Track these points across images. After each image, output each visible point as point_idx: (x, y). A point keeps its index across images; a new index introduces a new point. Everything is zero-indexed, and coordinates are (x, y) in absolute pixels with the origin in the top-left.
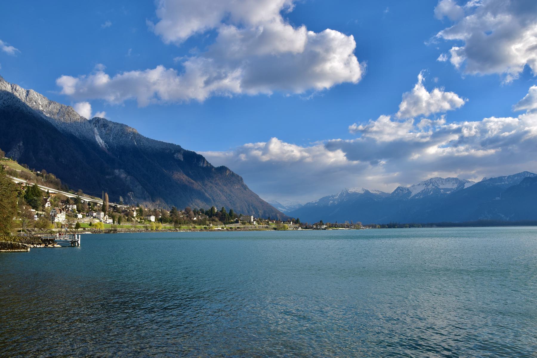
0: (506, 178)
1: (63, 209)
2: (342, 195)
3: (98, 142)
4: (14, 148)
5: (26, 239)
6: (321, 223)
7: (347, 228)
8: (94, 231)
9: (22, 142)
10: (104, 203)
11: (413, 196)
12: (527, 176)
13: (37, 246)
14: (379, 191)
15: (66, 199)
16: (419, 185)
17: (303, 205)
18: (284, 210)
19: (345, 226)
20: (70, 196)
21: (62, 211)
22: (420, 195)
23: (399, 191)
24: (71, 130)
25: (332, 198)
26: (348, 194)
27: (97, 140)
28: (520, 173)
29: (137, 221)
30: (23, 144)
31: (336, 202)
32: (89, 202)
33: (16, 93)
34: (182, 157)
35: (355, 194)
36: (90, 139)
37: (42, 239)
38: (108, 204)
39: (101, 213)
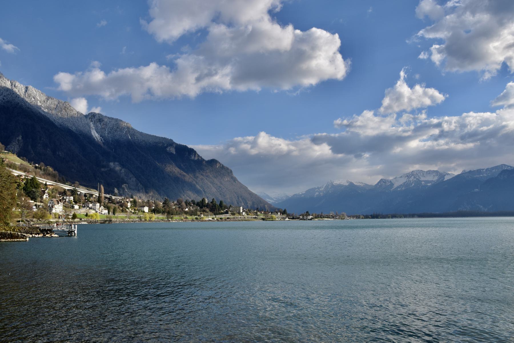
0: (484, 170)
1: (60, 201)
3: (94, 136)
5: (25, 230)
6: (308, 214)
7: (332, 218)
8: (90, 222)
9: (21, 136)
12: (504, 168)
13: (36, 236)
14: (362, 183)
16: (401, 177)
17: (290, 197)
19: (331, 216)
20: (67, 187)
21: (60, 202)
22: (402, 187)
24: (68, 125)
30: (22, 138)
31: (322, 194)
34: (174, 151)
35: (340, 186)
36: (86, 133)
37: (40, 229)
38: (103, 195)
39: (97, 204)
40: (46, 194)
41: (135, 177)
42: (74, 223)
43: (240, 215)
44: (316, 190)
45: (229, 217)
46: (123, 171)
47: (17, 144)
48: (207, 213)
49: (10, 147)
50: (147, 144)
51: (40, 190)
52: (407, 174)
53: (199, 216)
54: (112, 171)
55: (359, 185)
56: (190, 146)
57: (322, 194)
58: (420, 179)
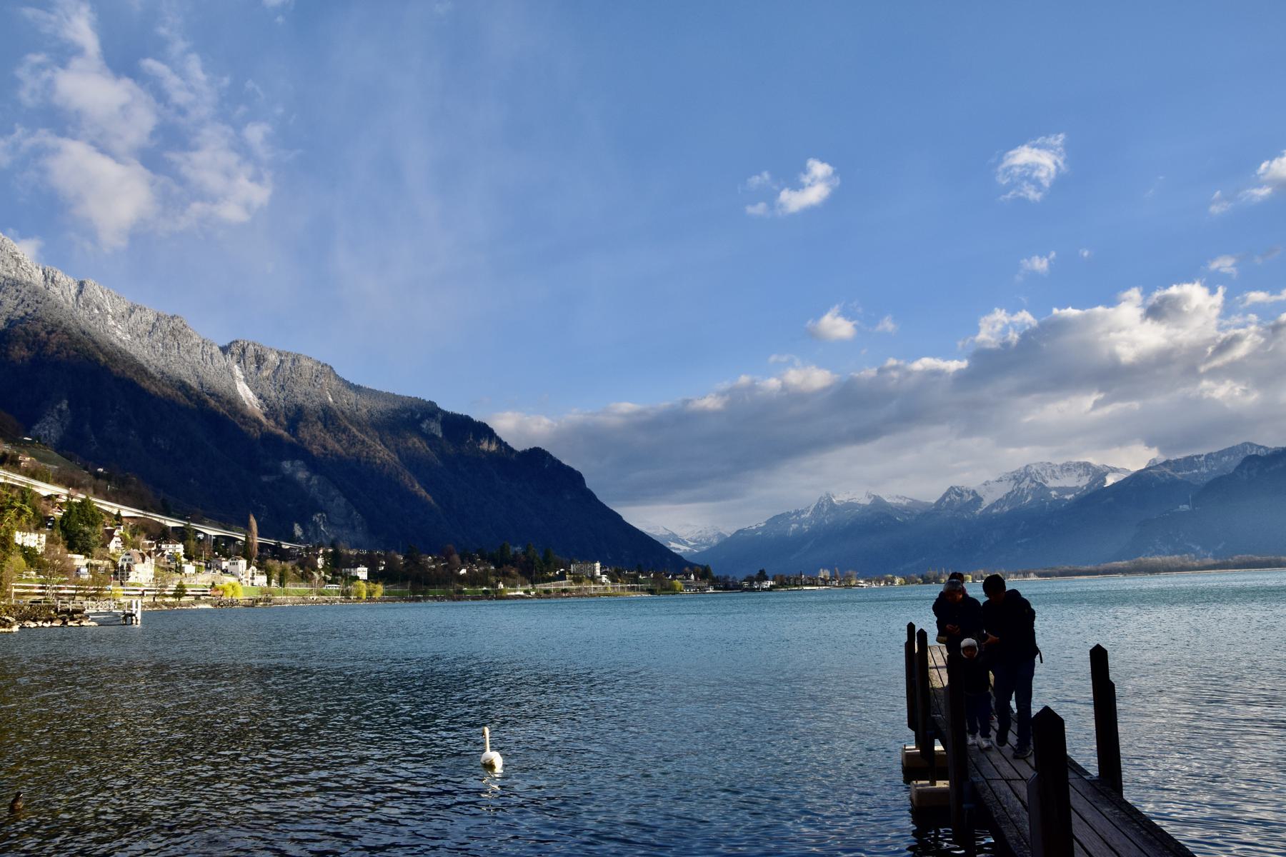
0: (1202, 459)
1: (149, 554)
2: (819, 507)
3: (244, 398)
4: (49, 415)
5: (20, 611)
6: (762, 577)
7: (822, 586)
8: (219, 603)
9: (66, 402)
10: (247, 537)
11: (986, 508)
12: (1251, 452)
13: (45, 625)
14: (906, 498)
15: (159, 532)
16: (1000, 480)
17: (729, 536)
18: (683, 548)
19: (819, 580)
20: (171, 523)
21: (147, 558)
22: (1002, 505)
23: (953, 496)
24: (181, 371)
25: (796, 518)
26: (833, 507)
27: (241, 393)
28: (1234, 447)
29: (325, 579)
30: (69, 405)
31: (806, 527)
32: (217, 536)
33: (55, 288)
34: (440, 430)
35: (850, 506)
36: (225, 392)
37: (56, 611)
38: (257, 540)
39: (240, 561)
40: (115, 539)
41: (345, 496)
42: (178, 607)
43: (594, 583)
44: (791, 519)
45: (567, 587)
46: (314, 480)
47: (58, 421)
48: (514, 578)
49: (40, 428)
50: (372, 415)
51: (101, 529)
52: (1012, 473)
53: (492, 586)
54: (289, 480)
55: (897, 503)
56: (477, 417)
57: (806, 527)
58: (1046, 485)
